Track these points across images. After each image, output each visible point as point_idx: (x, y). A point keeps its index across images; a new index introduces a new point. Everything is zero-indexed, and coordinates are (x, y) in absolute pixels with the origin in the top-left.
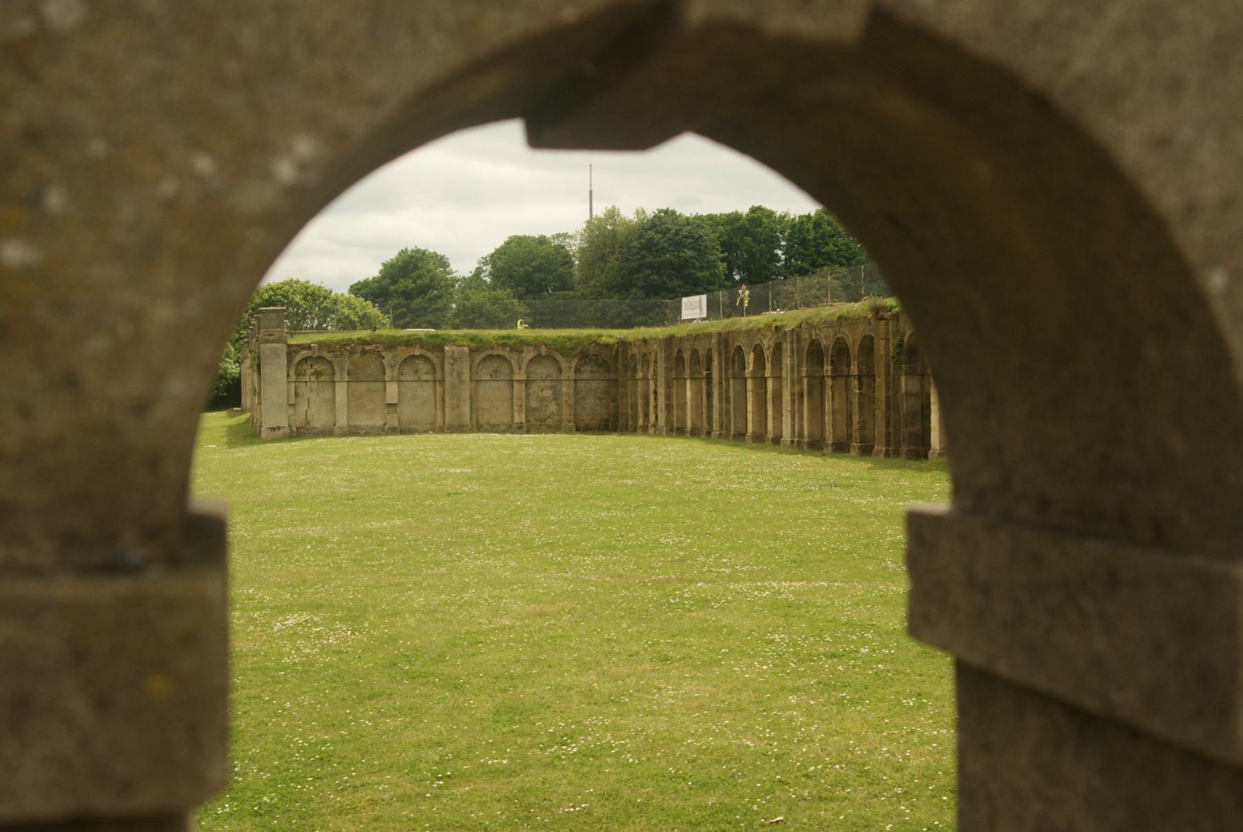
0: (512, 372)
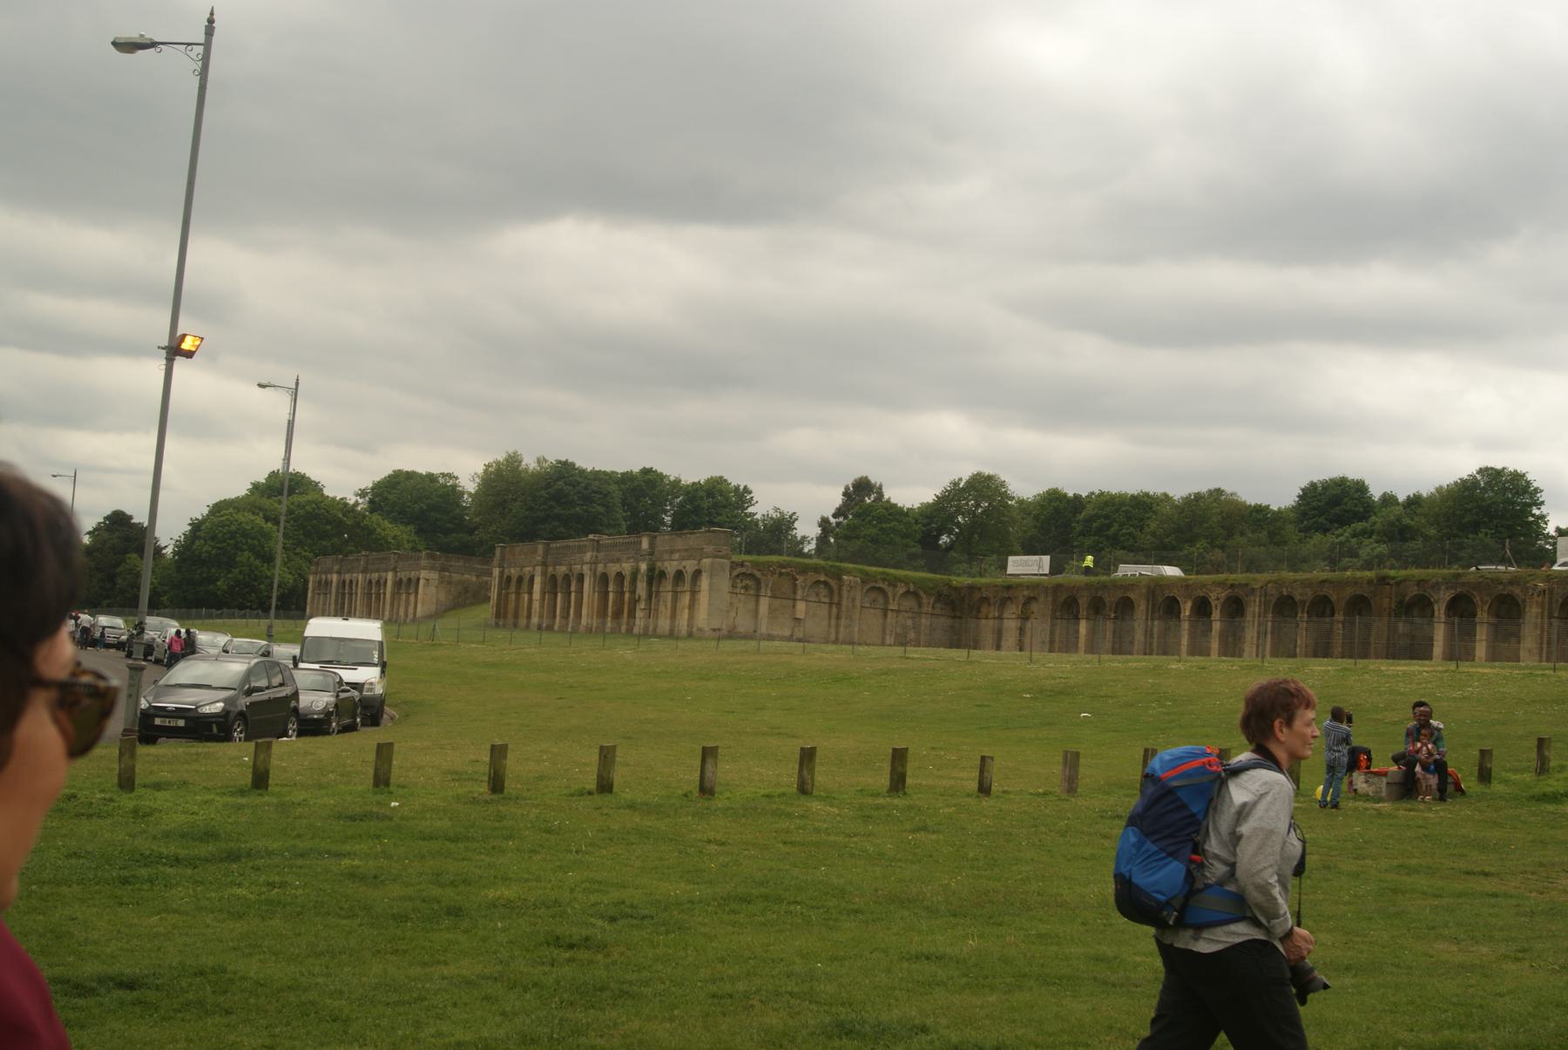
0: (887, 602)
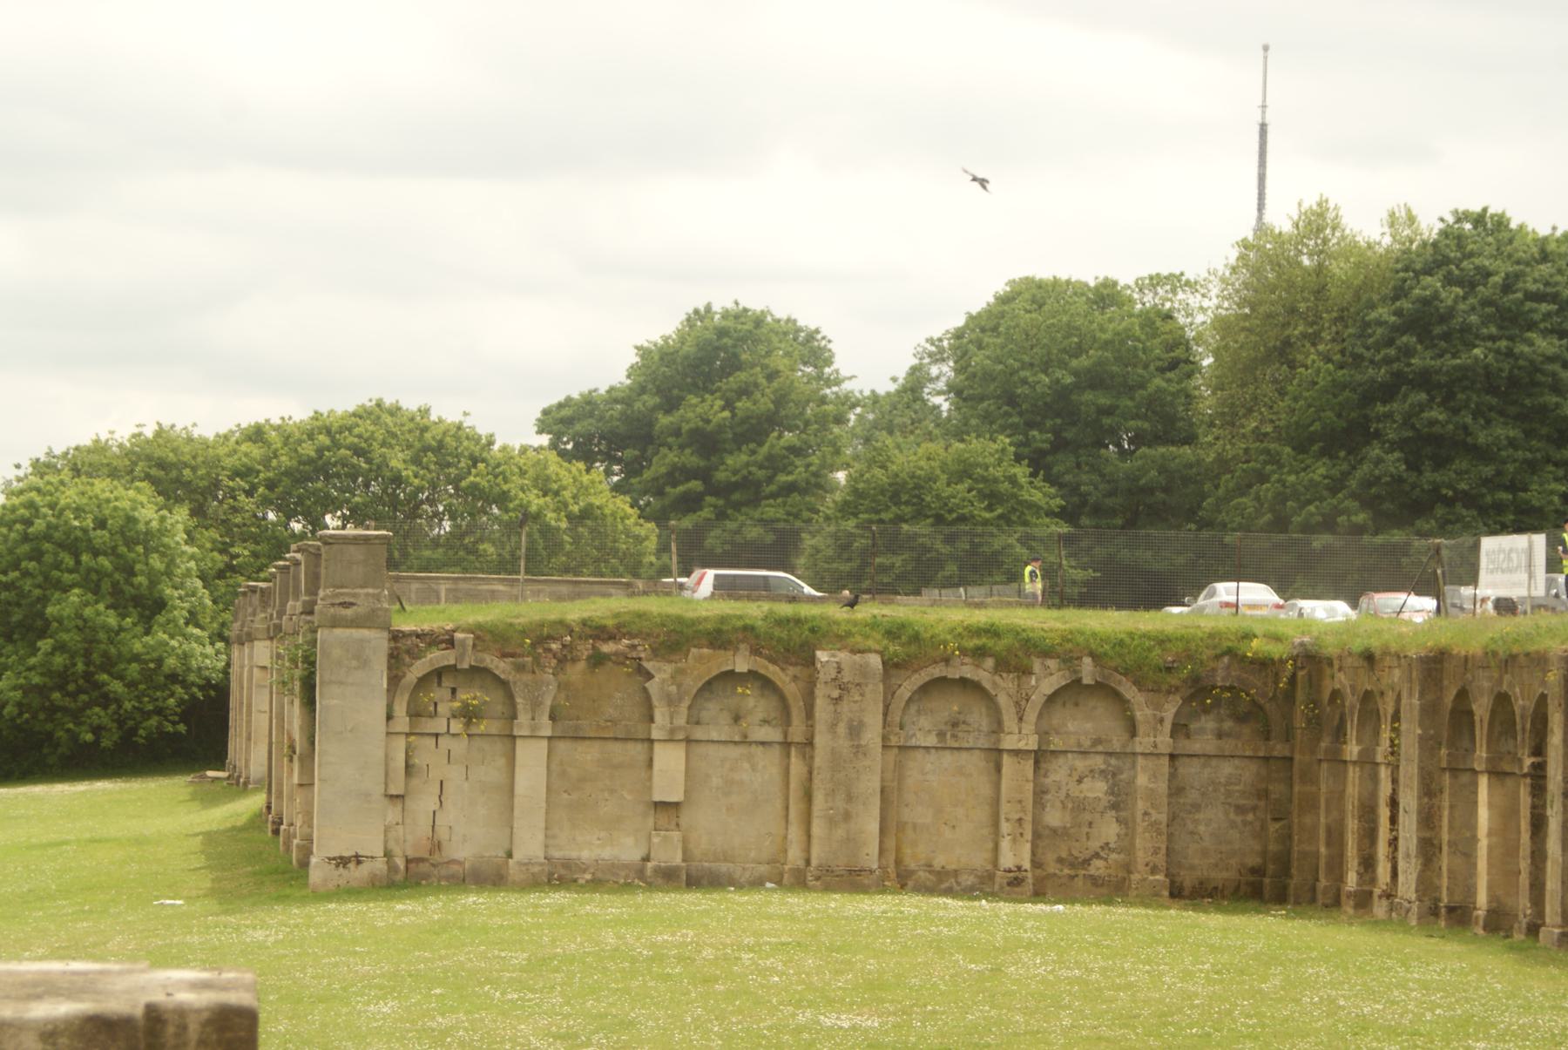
0: (998, 728)
